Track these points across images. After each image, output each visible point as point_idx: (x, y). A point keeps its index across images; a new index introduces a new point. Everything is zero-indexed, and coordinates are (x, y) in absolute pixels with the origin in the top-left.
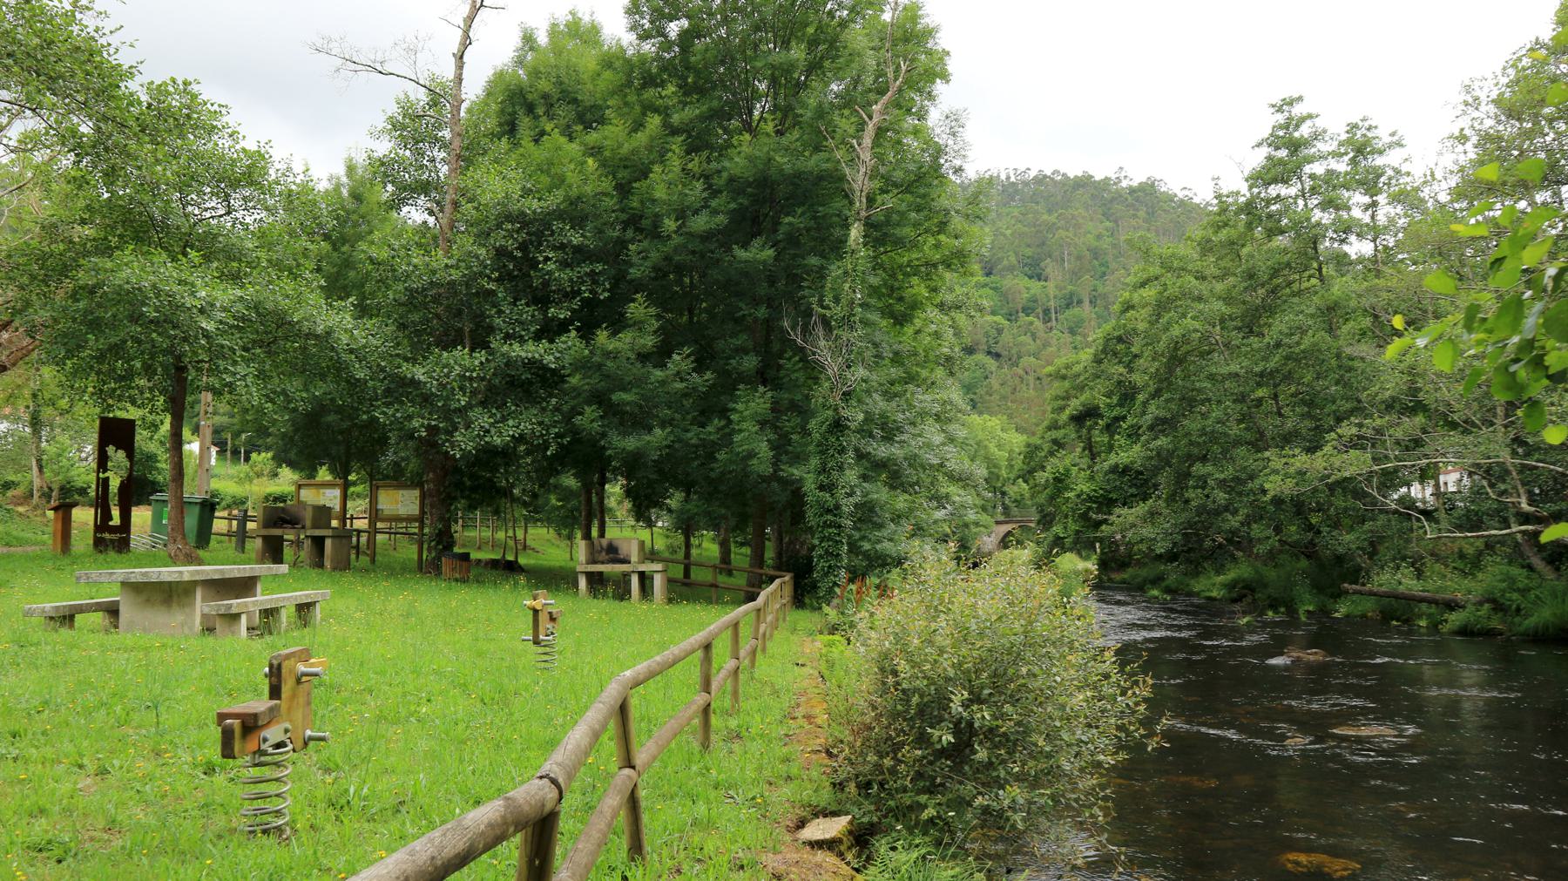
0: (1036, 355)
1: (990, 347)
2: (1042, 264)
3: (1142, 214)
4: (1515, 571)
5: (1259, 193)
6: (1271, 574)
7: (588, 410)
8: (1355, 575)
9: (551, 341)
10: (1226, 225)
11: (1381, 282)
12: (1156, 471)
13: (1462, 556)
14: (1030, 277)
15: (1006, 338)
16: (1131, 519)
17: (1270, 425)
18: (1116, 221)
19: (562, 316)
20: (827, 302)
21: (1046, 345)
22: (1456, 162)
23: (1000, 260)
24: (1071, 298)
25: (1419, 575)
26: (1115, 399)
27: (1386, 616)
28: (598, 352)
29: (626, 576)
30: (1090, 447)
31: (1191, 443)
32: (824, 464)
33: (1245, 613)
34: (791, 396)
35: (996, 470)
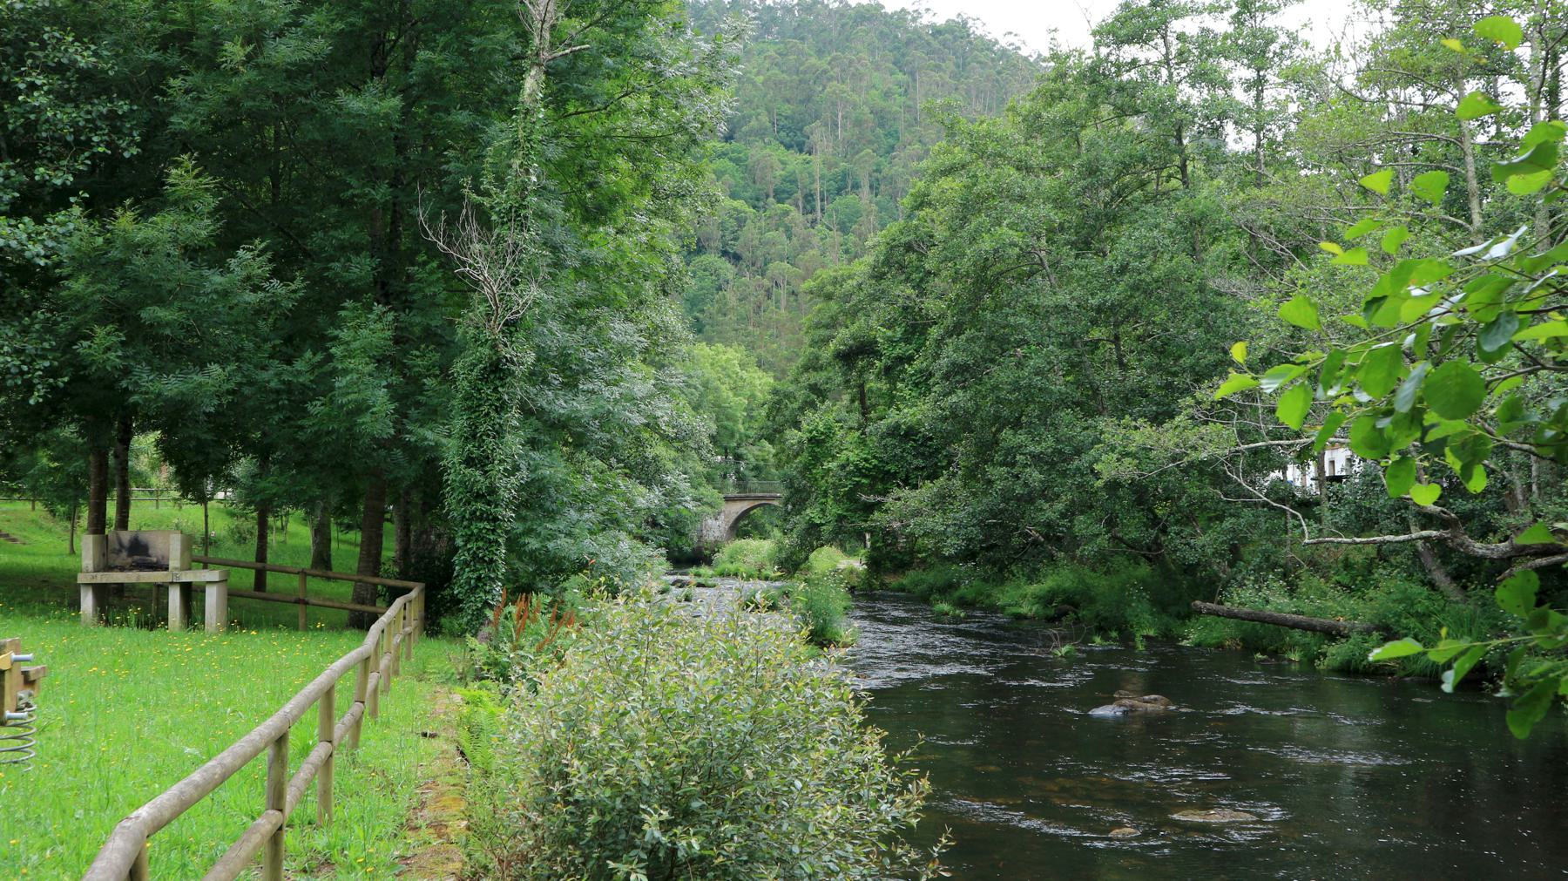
0: (791, 260)
1: (725, 244)
2: (807, 129)
3: (949, 66)
4: (1416, 589)
5: (1109, 54)
6: (1100, 583)
7: (100, 331)
8: (1211, 589)
9: (39, 220)
10: (1062, 96)
11: (1263, 193)
12: (949, 438)
13: (1347, 565)
14: (788, 147)
15: (750, 233)
16: (913, 504)
17: (1108, 379)
18: (912, 74)
19: (58, 182)
20: (485, 186)
21: (805, 245)
22: (1368, 35)
23: (746, 119)
24: (844, 179)
25: (1292, 590)
26: (899, 331)
27: (1250, 645)
28: (118, 243)
29: (162, 589)
30: (861, 396)
31: (999, 401)
32: (474, 427)
33: (1064, 640)
34: (425, 321)
35: (729, 424)
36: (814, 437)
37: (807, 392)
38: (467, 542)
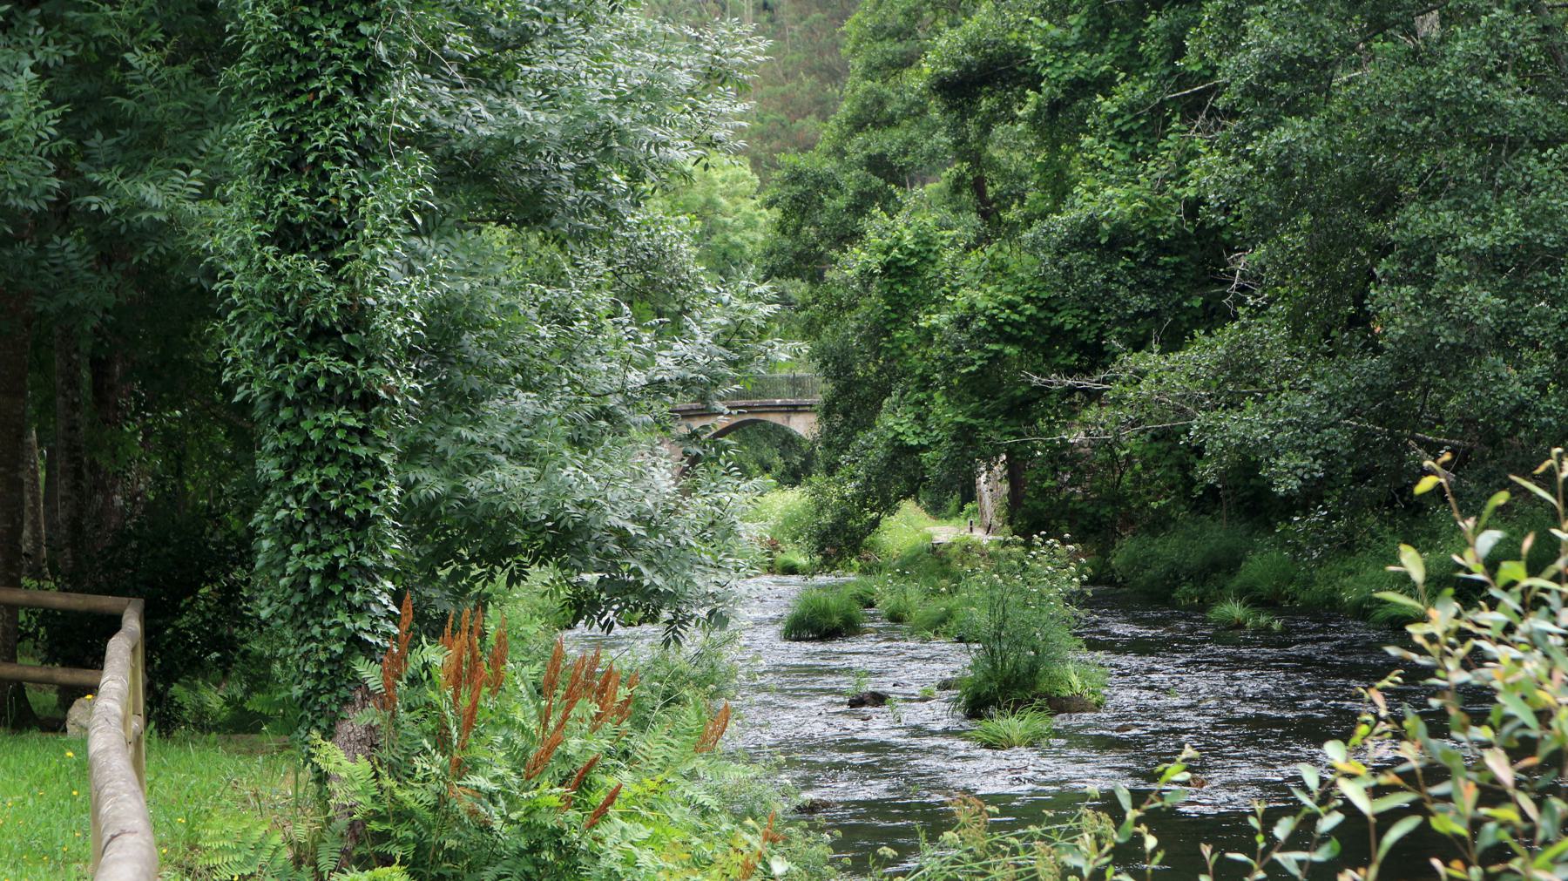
32: (295, 137)
36: (895, 261)
37: (862, 173)
38: (290, 469)
